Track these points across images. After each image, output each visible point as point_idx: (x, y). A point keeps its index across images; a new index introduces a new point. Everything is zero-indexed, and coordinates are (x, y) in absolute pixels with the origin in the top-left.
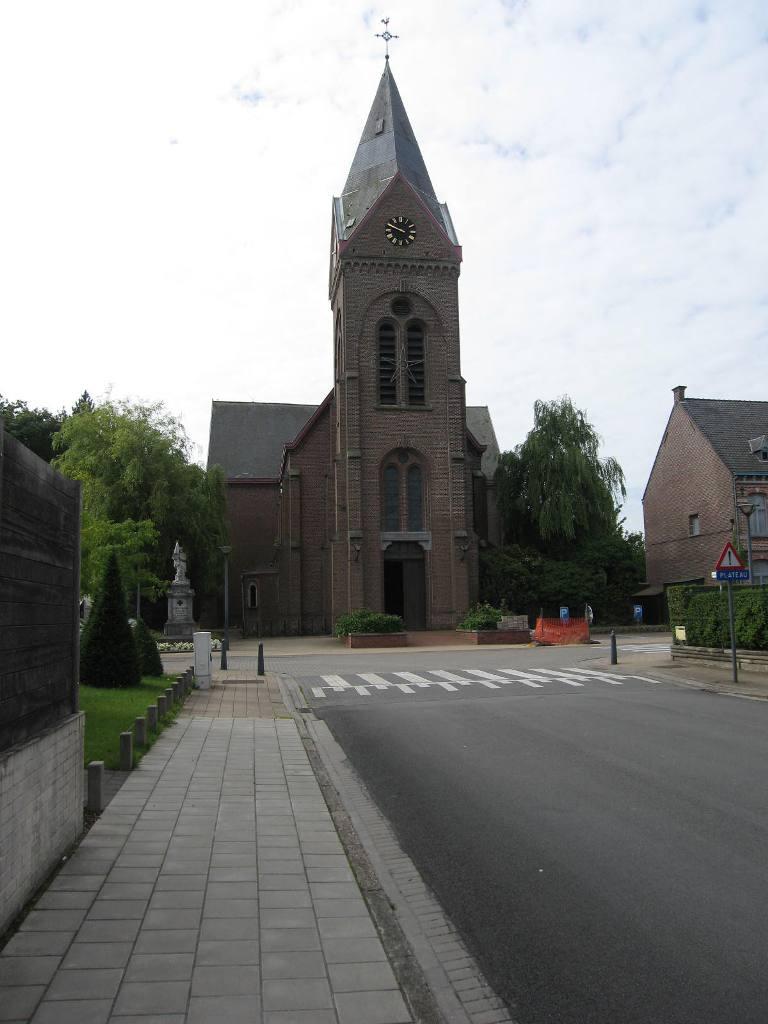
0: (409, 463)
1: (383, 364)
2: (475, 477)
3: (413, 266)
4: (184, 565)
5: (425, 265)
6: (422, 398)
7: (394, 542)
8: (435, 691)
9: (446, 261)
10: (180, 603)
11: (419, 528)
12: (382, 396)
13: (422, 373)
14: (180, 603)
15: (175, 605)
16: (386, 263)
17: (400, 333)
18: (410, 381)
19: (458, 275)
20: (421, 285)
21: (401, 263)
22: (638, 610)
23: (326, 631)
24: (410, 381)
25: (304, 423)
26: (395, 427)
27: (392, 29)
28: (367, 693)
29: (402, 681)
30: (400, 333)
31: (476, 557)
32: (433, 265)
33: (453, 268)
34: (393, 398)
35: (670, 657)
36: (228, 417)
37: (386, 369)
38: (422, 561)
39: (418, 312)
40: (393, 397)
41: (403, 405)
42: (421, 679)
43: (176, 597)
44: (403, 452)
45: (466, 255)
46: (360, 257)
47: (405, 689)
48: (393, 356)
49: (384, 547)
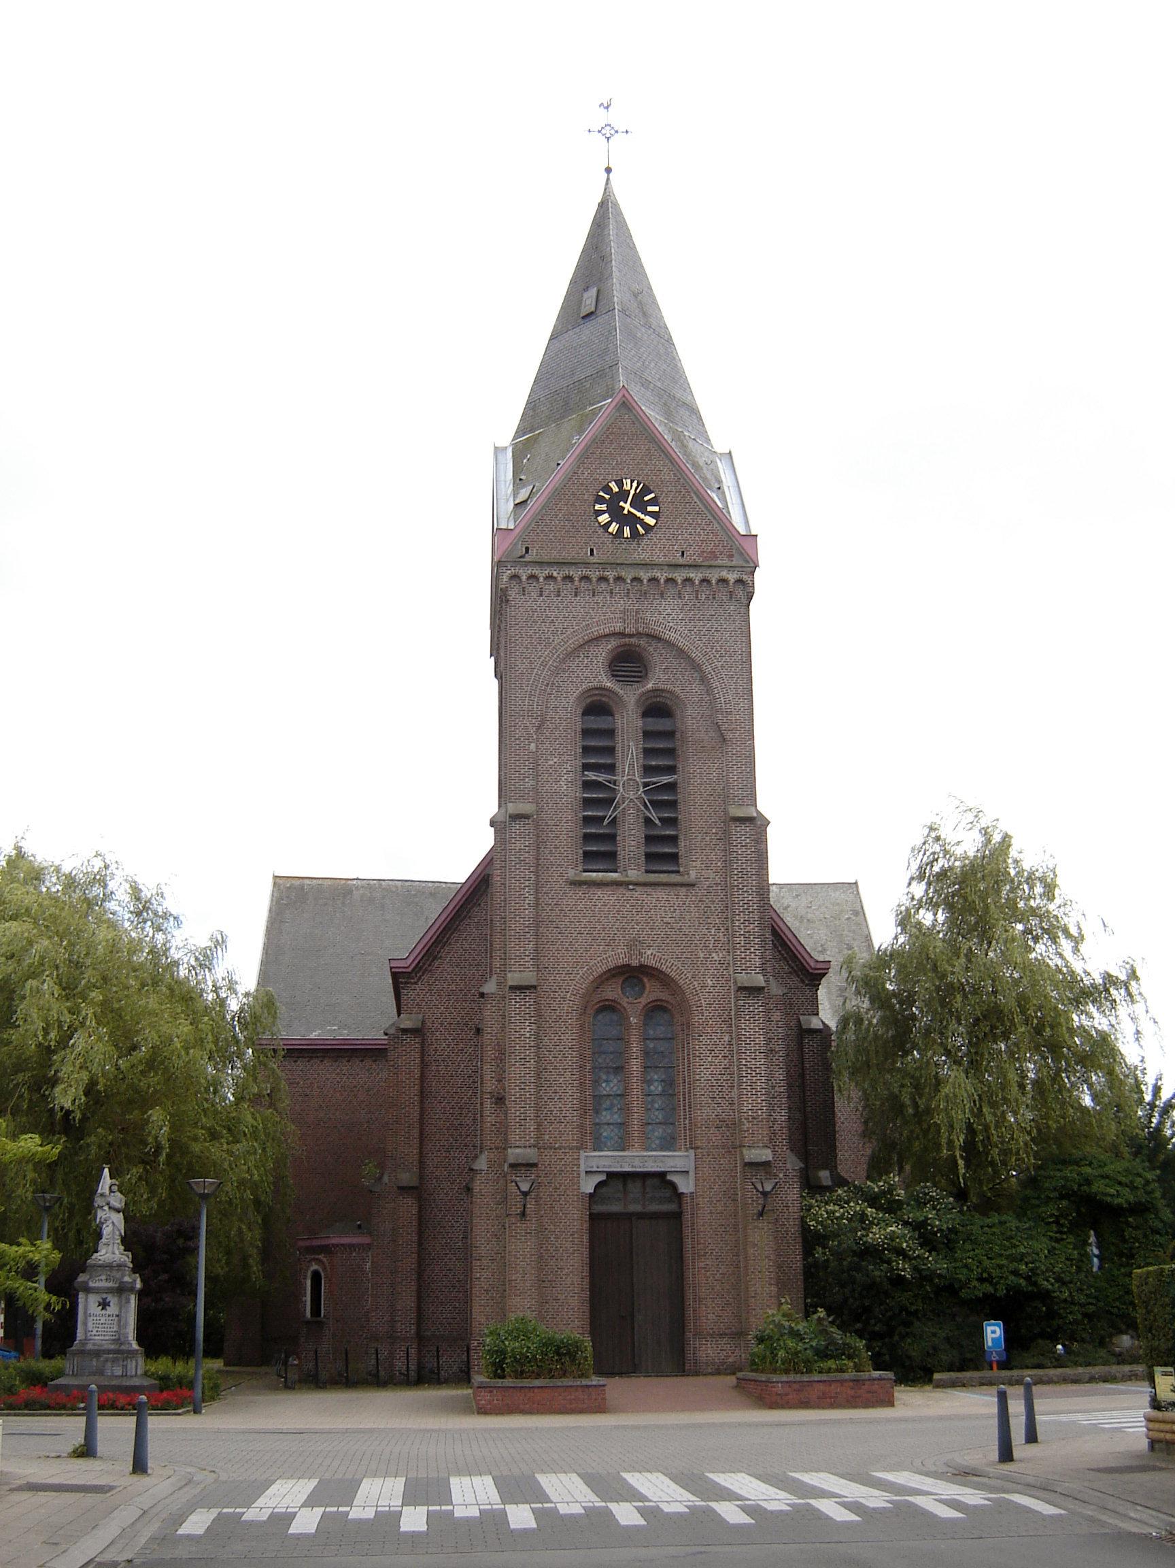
0: (644, 1000)
1: (587, 785)
2: (804, 1033)
3: (653, 580)
4: (118, 1219)
5: (679, 576)
6: (674, 857)
7: (610, 1175)
8: (804, 1520)
9: (725, 572)
10: (104, 1305)
11: (669, 1143)
12: (587, 854)
13: (673, 804)
14: (104, 1305)
15: (94, 1308)
16: (594, 575)
17: (629, 724)
18: (648, 821)
19: (750, 596)
20: (668, 617)
21: (628, 575)
22: (993, 1332)
23: (463, 1377)
24: (648, 821)
25: (434, 912)
26: (605, 922)
27: (615, 117)
28: (745, 1519)
29: (727, 1495)
30: (629, 724)
31: (794, 1209)
32: (696, 576)
33: (740, 581)
34: (609, 858)
35: (1144, 1444)
36: (299, 905)
37: (597, 797)
38: (677, 1216)
39: (662, 676)
40: (612, 856)
41: (634, 874)
42: (772, 1491)
43: (97, 1291)
44: (633, 975)
45: (765, 553)
46: (540, 564)
47: (730, 1513)
48: (611, 769)
49: (588, 1186)
